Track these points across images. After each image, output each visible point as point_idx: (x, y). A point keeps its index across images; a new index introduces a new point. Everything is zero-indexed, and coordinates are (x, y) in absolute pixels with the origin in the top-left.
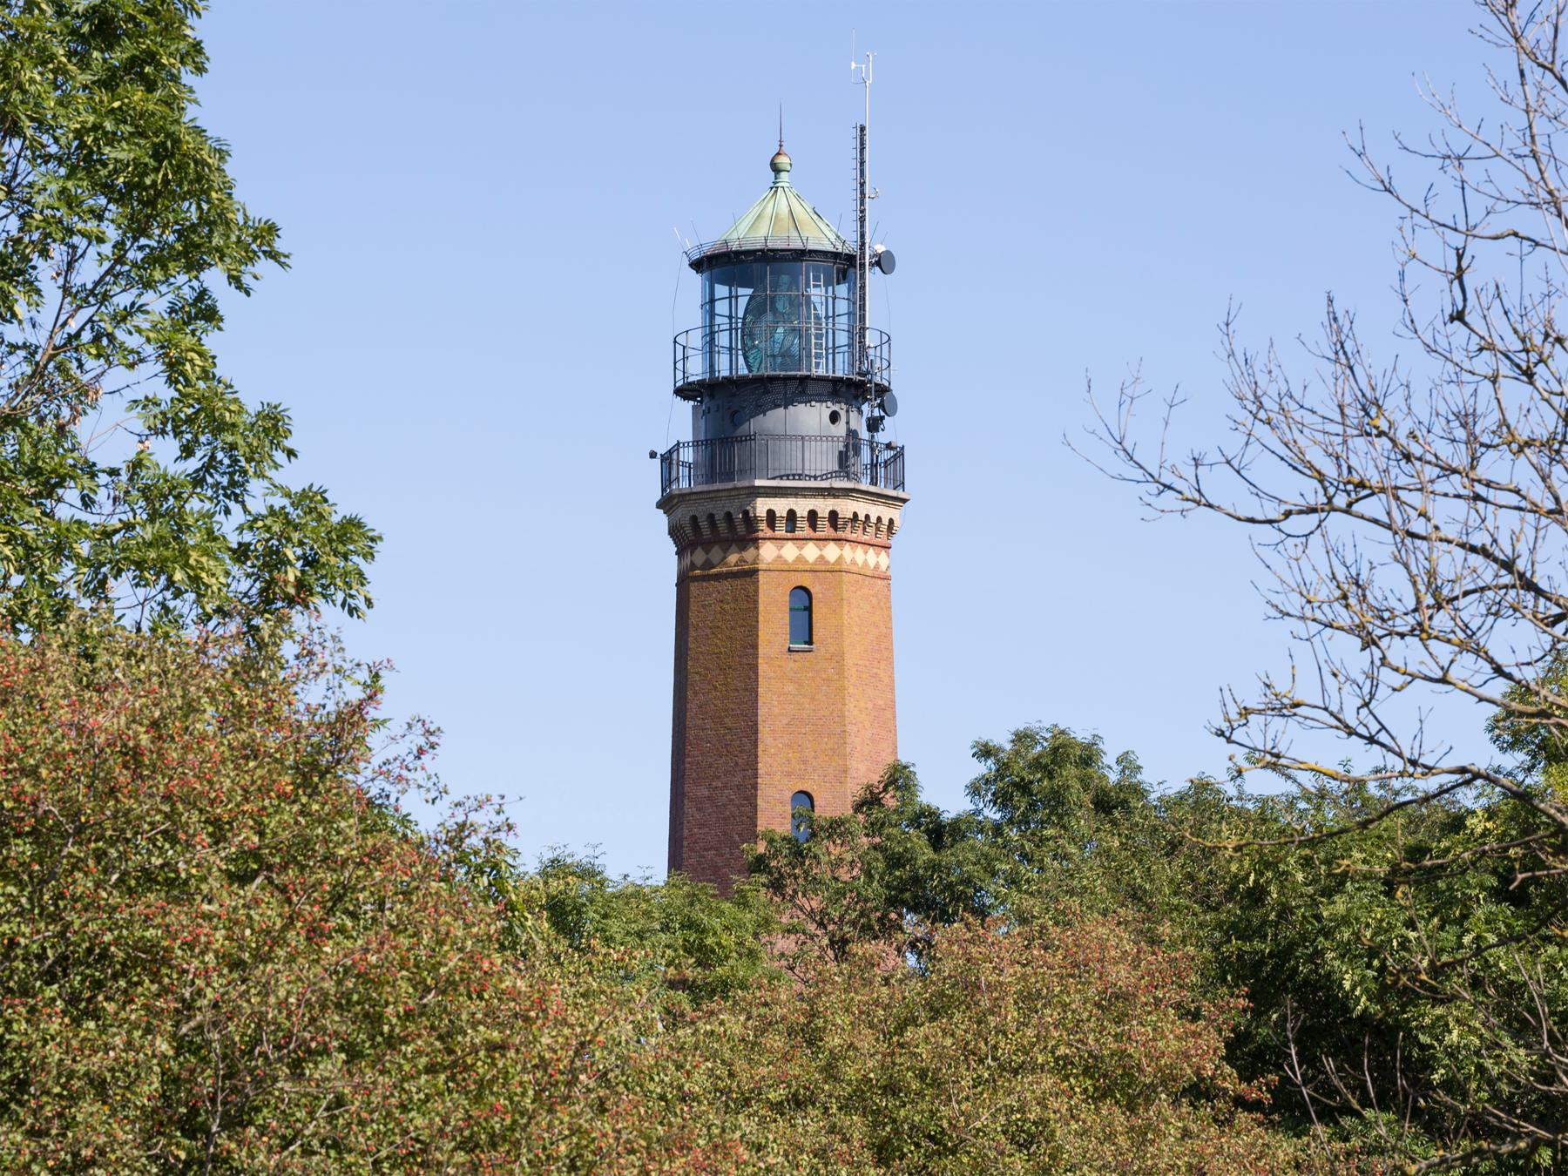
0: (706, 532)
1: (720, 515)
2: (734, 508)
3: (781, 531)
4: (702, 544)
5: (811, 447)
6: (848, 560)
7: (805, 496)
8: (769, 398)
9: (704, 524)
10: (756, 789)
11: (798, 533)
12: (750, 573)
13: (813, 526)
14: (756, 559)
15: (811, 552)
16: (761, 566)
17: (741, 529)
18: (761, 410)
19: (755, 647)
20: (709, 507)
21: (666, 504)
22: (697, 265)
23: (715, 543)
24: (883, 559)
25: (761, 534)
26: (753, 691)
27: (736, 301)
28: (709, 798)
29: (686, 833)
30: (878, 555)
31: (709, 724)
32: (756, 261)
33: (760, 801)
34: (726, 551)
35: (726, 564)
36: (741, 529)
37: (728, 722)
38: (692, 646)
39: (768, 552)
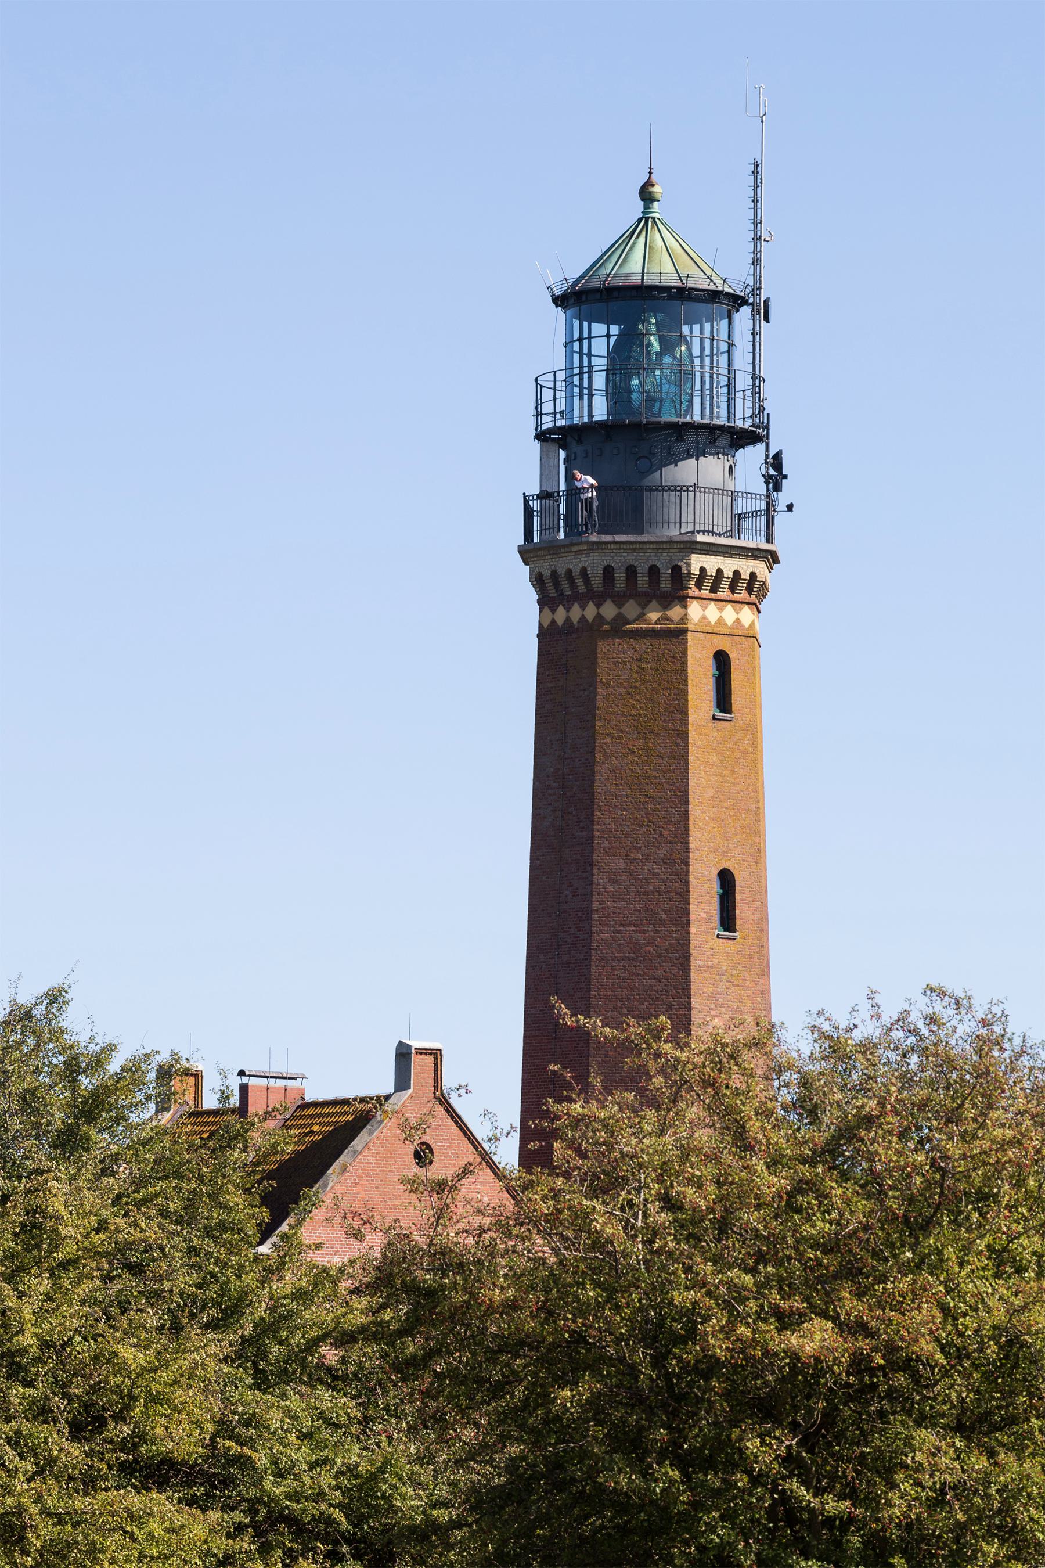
0: (643, 580)
1: (642, 568)
2: (663, 563)
3: (724, 594)
4: (610, 597)
5: (703, 498)
6: (730, 622)
7: (731, 556)
8: (681, 447)
9: (620, 576)
10: (687, 864)
11: (720, 595)
12: (679, 633)
13: (733, 588)
14: (684, 619)
15: (729, 614)
16: (690, 627)
17: (665, 585)
18: (674, 459)
19: (684, 712)
20: (630, 559)
21: (526, 553)
22: (560, 301)
23: (631, 597)
24: (746, 615)
25: (690, 593)
26: (683, 759)
27: (601, 336)
28: (625, 870)
29: (595, 905)
30: (721, 610)
31: (624, 790)
32: (671, 297)
33: (692, 879)
34: (644, 606)
35: (646, 622)
36: (665, 585)
37: (650, 789)
38: (600, 704)
39: (695, 611)
